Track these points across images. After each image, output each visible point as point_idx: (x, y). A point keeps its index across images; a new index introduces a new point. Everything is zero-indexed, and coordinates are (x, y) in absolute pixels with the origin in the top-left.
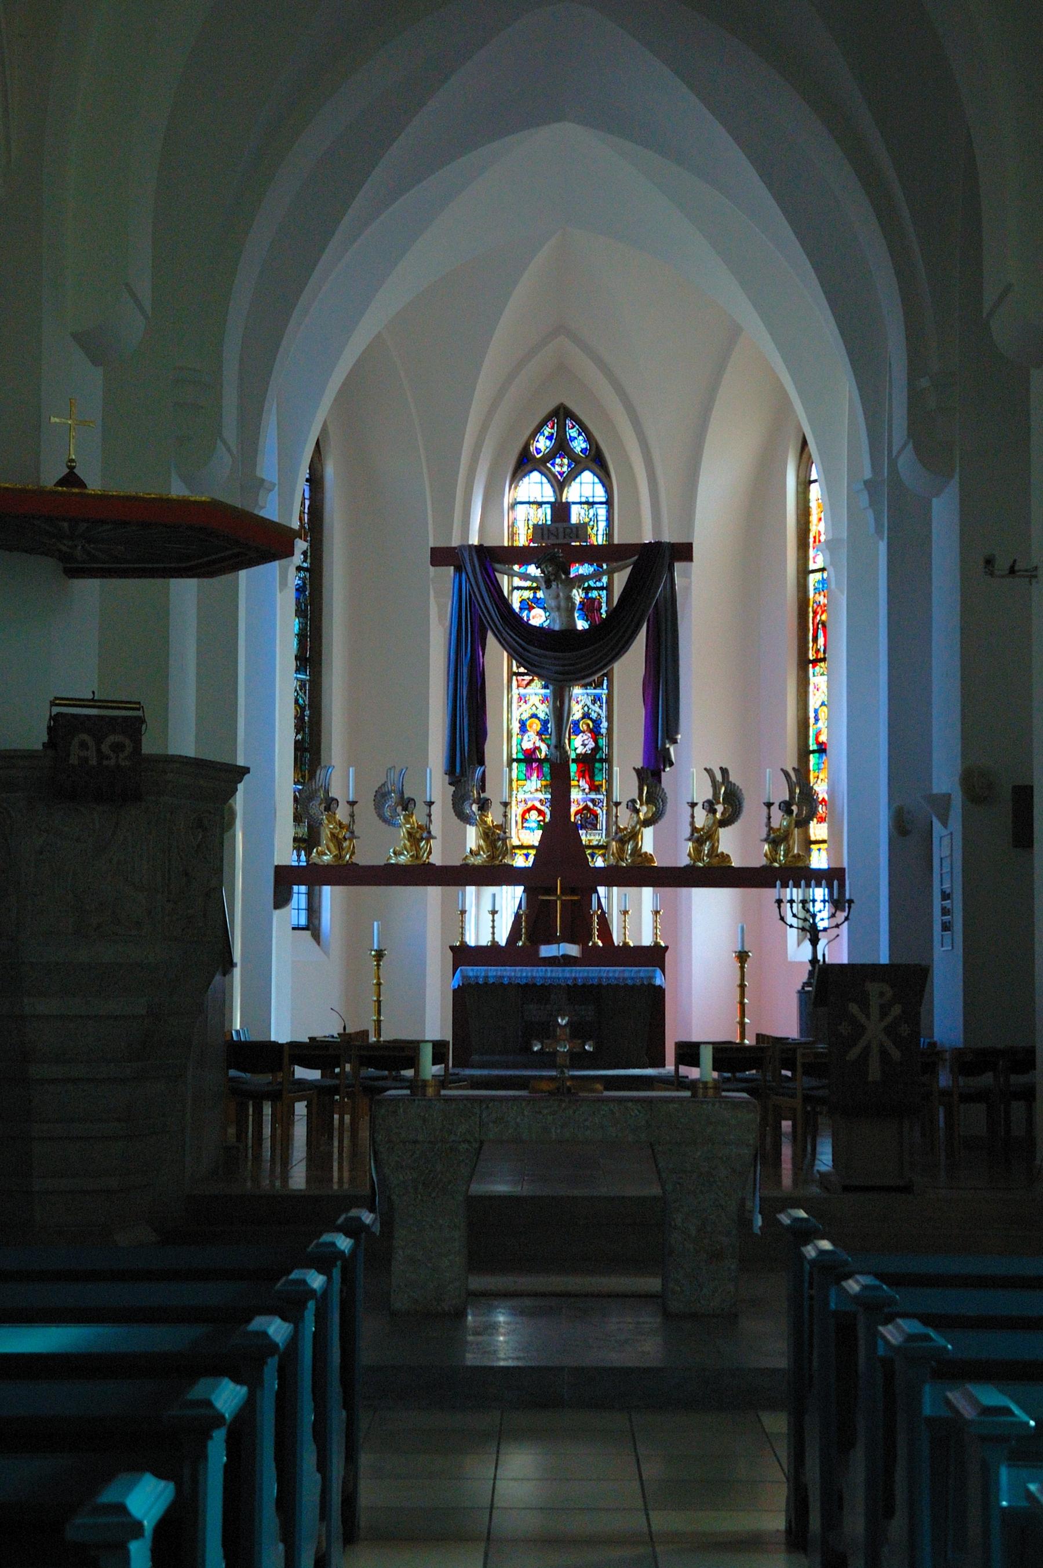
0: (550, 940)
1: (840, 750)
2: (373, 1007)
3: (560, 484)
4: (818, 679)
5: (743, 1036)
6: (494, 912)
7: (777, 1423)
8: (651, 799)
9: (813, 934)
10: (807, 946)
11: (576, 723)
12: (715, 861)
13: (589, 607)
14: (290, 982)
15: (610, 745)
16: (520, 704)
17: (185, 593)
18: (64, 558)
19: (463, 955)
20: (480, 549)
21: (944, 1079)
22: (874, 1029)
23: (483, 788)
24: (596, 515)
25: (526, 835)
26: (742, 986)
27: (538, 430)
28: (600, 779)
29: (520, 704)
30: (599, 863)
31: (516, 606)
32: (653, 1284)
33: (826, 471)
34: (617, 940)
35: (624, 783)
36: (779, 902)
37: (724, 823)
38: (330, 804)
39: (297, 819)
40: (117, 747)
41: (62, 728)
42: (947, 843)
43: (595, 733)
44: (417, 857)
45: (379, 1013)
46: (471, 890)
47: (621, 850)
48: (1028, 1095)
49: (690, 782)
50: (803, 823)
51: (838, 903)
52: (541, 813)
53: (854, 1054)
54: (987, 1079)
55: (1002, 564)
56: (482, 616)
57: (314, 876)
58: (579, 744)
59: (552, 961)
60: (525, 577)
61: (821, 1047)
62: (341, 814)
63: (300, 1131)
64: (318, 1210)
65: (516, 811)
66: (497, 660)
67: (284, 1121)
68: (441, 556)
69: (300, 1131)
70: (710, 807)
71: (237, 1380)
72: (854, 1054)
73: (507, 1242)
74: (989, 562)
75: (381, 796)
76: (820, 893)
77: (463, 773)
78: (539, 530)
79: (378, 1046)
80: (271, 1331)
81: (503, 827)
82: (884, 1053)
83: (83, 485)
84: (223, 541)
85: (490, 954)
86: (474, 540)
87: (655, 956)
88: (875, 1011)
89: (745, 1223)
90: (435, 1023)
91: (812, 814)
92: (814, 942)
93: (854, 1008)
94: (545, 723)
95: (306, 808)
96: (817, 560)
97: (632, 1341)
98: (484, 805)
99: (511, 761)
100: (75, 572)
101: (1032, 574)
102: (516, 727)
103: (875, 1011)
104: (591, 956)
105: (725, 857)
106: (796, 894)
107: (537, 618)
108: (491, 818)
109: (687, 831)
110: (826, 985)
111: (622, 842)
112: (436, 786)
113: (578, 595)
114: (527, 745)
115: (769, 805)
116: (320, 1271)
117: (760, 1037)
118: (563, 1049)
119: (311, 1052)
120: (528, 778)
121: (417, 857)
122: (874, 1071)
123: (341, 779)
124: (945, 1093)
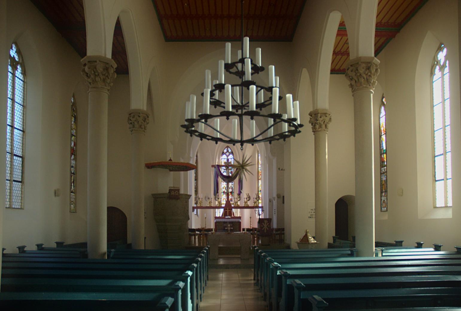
0: (227, 216)
1: (263, 191)
2: (205, 225)
3: (227, 156)
4: (260, 181)
5: (251, 227)
6: (220, 212)
7: (253, 270)
8: (239, 198)
9: (259, 215)
10: (259, 216)
11: (230, 188)
12: (247, 206)
13: (231, 172)
14: (195, 223)
15: (234, 190)
16: (223, 185)
17: (182, 173)
18: (170, 169)
19: (216, 218)
20: (218, 165)
21: (274, 232)
22: (265, 226)
23: (218, 196)
24: (232, 160)
25: (224, 202)
26: (251, 222)
27: (225, 149)
28: (233, 195)
29: (223, 185)
30: (233, 206)
31: (222, 172)
32: (240, 256)
33: (261, 154)
34: (235, 216)
35: (236, 195)
36: (255, 211)
37: (248, 200)
38: (199, 199)
39: (195, 200)
40: (177, 193)
41: (170, 190)
42: (275, 203)
43: (232, 189)
44: (210, 205)
45: (206, 225)
46: (217, 210)
47: (236, 204)
48: (284, 234)
49: (244, 195)
50: (258, 200)
51: (262, 211)
52: (225, 199)
53: (263, 229)
54: (279, 232)
55: (281, 169)
56: (219, 174)
57: (197, 208)
58: (230, 190)
59: (227, 218)
60: (223, 168)
61: (260, 229)
62: (201, 200)
63: (197, 240)
64: (200, 249)
65: (222, 199)
66: (220, 179)
67: (195, 238)
68: (213, 166)
69: (197, 240)
70: (247, 199)
71: (172, 297)
72: (263, 229)
73: (223, 252)
74: (279, 169)
75: (206, 198)
76: (260, 209)
77: (216, 194)
78: (225, 163)
79: (206, 229)
80: (180, 285)
81: (221, 201)
82: (267, 229)
83: (172, 161)
84: (187, 167)
85: (219, 218)
86: (217, 164)
87: (240, 218)
88: (265, 224)
89: (250, 248)
90: (212, 226)
91: (259, 199)
92: (259, 216)
93: (263, 224)
94: (226, 188)
95: (196, 199)
96: (260, 166)
97: (238, 262)
98: (218, 199)
99: (221, 192)
100: (170, 171)
101: (284, 170)
102: (222, 188)
103: (265, 224)
104: (232, 218)
105: (248, 205)
106: (257, 209)
107: (225, 174)
108: (219, 200)
109: (244, 201)
110: (261, 221)
111: (236, 203)
112: (212, 196)
113: (230, 171)
114: (224, 190)
115: (254, 198)
116: (191, 271)
117: (253, 228)
118: (229, 229)
119: (198, 230)
120: (224, 195)
121: (210, 205)
122: (265, 231)
123: (200, 195)
124: (274, 234)
